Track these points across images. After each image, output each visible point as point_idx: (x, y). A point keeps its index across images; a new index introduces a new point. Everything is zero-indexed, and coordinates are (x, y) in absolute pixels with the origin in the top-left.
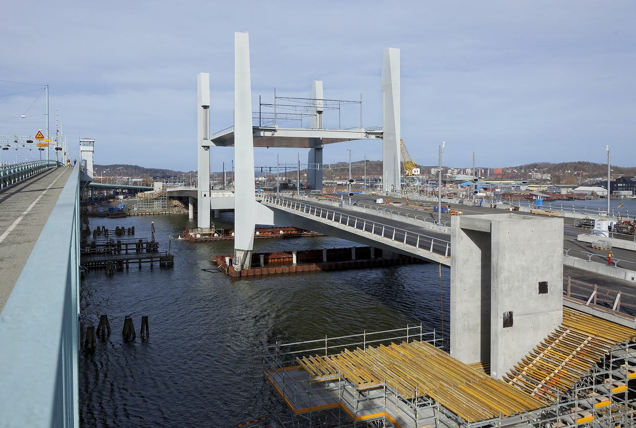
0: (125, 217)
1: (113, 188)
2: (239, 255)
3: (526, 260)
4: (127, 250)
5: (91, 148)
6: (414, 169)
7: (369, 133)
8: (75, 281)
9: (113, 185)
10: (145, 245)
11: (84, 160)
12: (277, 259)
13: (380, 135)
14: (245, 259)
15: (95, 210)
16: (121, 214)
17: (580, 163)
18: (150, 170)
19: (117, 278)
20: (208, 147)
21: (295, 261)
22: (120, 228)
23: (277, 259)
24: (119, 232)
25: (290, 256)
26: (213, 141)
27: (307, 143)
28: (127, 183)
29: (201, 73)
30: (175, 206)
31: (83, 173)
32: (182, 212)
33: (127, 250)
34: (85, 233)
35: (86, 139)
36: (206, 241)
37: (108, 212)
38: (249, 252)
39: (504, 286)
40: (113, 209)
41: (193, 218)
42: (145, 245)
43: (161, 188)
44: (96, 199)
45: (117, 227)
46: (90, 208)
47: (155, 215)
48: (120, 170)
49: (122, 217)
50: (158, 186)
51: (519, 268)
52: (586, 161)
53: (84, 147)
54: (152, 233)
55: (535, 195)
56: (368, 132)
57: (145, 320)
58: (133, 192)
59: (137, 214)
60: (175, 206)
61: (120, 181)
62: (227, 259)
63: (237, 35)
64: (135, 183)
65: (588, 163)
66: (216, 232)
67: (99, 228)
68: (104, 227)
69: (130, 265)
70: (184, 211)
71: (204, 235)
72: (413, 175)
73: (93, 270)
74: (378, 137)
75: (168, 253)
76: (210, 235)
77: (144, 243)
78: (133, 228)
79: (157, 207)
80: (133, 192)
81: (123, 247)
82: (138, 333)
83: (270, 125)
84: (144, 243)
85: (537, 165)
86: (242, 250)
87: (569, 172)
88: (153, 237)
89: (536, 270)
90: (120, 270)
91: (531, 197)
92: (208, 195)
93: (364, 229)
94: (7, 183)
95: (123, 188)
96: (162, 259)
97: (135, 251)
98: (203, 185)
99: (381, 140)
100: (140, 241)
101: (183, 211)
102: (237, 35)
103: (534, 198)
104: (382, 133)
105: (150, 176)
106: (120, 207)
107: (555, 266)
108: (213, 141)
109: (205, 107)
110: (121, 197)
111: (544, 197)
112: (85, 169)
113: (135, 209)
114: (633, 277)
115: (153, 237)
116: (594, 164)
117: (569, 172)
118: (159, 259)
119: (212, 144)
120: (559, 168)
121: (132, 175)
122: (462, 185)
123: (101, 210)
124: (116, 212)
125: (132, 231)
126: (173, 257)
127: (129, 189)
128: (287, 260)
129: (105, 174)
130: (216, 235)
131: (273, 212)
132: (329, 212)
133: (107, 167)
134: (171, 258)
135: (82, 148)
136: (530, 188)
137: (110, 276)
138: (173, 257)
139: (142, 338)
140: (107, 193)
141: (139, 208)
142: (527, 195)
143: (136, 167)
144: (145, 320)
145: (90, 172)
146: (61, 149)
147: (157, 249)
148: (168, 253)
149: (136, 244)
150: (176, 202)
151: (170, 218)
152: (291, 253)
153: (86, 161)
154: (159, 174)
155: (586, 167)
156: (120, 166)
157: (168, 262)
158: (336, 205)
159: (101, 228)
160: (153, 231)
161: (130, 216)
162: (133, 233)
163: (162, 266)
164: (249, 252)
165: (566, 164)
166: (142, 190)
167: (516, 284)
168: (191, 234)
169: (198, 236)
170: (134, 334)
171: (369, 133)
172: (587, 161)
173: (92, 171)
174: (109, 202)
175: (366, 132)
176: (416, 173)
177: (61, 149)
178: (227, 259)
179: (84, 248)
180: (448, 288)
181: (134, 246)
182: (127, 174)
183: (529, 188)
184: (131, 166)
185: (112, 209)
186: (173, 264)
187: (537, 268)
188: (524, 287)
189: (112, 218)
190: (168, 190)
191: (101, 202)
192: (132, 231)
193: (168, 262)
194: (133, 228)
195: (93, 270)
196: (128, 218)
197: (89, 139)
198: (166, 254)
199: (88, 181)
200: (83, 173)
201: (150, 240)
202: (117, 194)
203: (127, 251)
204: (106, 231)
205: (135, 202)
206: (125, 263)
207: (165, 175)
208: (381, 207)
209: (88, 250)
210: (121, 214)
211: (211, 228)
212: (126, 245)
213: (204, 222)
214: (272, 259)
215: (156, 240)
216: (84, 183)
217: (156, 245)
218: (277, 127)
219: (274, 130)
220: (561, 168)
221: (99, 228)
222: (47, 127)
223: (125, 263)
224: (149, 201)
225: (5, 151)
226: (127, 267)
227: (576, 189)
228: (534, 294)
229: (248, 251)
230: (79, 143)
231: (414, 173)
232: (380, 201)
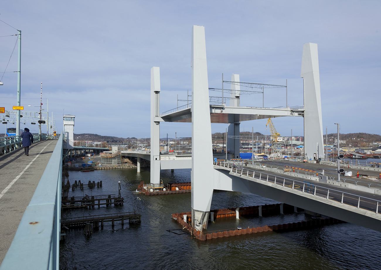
0: (93, 171)
1: (84, 149)
2: (198, 216)
4: (99, 205)
5: (72, 123)
6: (278, 138)
7: (294, 111)
8: (59, 202)
9: (84, 147)
10: (113, 201)
11: (66, 132)
12: (223, 214)
13: (302, 113)
14: (203, 219)
15: (73, 166)
16: (90, 169)
17: (360, 134)
19: (95, 238)
20: (159, 122)
21: (238, 217)
22: (92, 182)
23: (223, 214)
24: (91, 186)
25: (233, 212)
26: (163, 118)
27: (227, 118)
29: (154, 67)
30: (126, 163)
31: (65, 143)
32: (131, 167)
33: (99, 205)
34: (65, 188)
35: (69, 115)
36: (158, 195)
37: (82, 167)
38: (207, 214)
40: (85, 165)
41: (140, 172)
43: (117, 151)
44: (73, 156)
45: (90, 182)
46: (69, 164)
47: (114, 170)
49: (91, 171)
50: (115, 149)
52: (364, 132)
53: (67, 122)
54: (119, 190)
55: (354, 155)
56: (293, 110)
58: (97, 152)
59: (101, 168)
60: (126, 163)
61: (88, 143)
62: (185, 217)
63: (196, 27)
64: (97, 145)
65: (365, 134)
66: (164, 187)
67: (76, 182)
68: (80, 181)
70: (133, 166)
71: (156, 189)
72: (278, 141)
73: (73, 230)
74: (300, 114)
76: (160, 189)
78: (101, 182)
79: (114, 164)
80: (97, 152)
81: (96, 202)
83: (220, 105)
85: (333, 135)
86: (201, 211)
87: (354, 139)
88: (120, 193)
90: (96, 229)
92: (158, 159)
94: (10, 150)
95: (90, 149)
97: (105, 206)
98: (154, 151)
101: (133, 166)
102: (196, 27)
103: (354, 157)
104: (303, 112)
105: (105, 140)
106: (89, 163)
108: (163, 118)
109: (157, 92)
110: (89, 155)
111: (360, 156)
112: (68, 140)
113: (100, 165)
115: (120, 193)
116: (369, 134)
117: (354, 139)
119: (161, 120)
120: (348, 137)
121: (94, 140)
122: (297, 147)
123: (77, 165)
124: (87, 167)
125: (100, 185)
127: (94, 150)
128: (231, 215)
129: (78, 139)
130: (164, 189)
131: (232, 179)
132: (277, 177)
133: (79, 135)
134: (138, 217)
135: (65, 122)
136: (344, 150)
137: (88, 237)
140: (80, 152)
141: (102, 164)
142: (349, 155)
143: (96, 135)
145: (71, 142)
146: (44, 122)
147: (123, 203)
150: (126, 160)
151: (123, 172)
152: (234, 210)
153: (68, 133)
154: (109, 140)
155: (365, 136)
156: (87, 134)
158: (315, 179)
159: (78, 182)
160: (120, 189)
161: (96, 169)
162: (101, 186)
163: (131, 224)
164: (207, 214)
165: (352, 134)
168: (145, 188)
169: (152, 190)
171: (294, 111)
172: (365, 133)
173: (73, 141)
174: (82, 159)
175: (292, 111)
176: (279, 141)
177: (44, 122)
178: (185, 217)
179: (65, 204)
180: (190, 175)
181: (105, 202)
182: (90, 140)
183: (342, 150)
184: (93, 135)
185: (84, 165)
186: (140, 222)
189: (84, 172)
190: (122, 152)
191: (76, 159)
192: (100, 185)
194: (101, 182)
195: (73, 230)
196: (95, 171)
197: (70, 115)
199: (69, 149)
200: (65, 143)
201: (117, 196)
202: (87, 153)
203: (99, 206)
204: (82, 185)
205: (99, 159)
206: (100, 222)
207: (114, 141)
208: (350, 180)
209: (68, 205)
210: (90, 169)
211: (160, 184)
212: (99, 200)
213: (155, 178)
214: (219, 215)
215: (122, 196)
216: (65, 150)
217: (122, 200)
218: (225, 105)
219: (222, 108)
220: (349, 137)
221: (76, 182)
222: (18, 90)
224: (109, 159)
225: (33, 125)
226: (102, 226)
227: (376, 151)
229: (206, 212)
230: (63, 118)
231: (278, 141)
232: (349, 174)
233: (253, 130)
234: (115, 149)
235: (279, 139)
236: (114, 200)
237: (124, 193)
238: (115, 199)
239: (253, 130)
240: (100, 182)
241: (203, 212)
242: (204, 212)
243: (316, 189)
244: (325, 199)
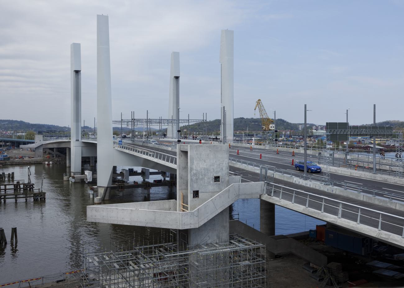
3: (206, 165)
4: (5, 190)
10: (22, 186)
18: (35, 125)
28: (11, 137)
33: (5, 190)
39: (193, 178)
42: (22, 186)
48: (4, 125)
51: (202, 169)
54: (29, 175)
57: (14, 230)
64: (20, 137)
69: (8, 201)
72: (270, 130)
75: (40, 190)
77: (21, 184)
82: (8, 239)
84: (21, 184)
86: (103, 187)
88: (29, 179)
89: (212, 170)
91: (369, 149)
93: (170, 162)
96: (35, 195)
99: (263, 102)
100: (18, 182)
107: (224, 168)
114: (398, 205)
115: (29, 179)
118: (33, 195)
126: (45, 193)
138: (45, 193)
139: (12, 245)
143: (21, 123)
144: (14, 230)
147: (33, 189)
148: (40, 190)
149: (14, 185)
157: (41, 197)
160: (29, 174)
163: (36, 201)
164: (109, 188)
166: (25, 143)
167: (201, 177)
170: (5, 240)
176: (272, 128)
187: (213, 169)
188: (206, 178)
193: (41, 197)
198: (39, 191)
206: (2, 198)
217: (32, 186)
223: (2, 198)
226: (5, 201)
228: (212, 182)
231: (271, 129)
233: (275, 118)
234: (39, 140)
235: (271, 127)
236: (23, 185)
237: (88, 278)
238: (24, 184)
239: (275, 118)
240: (11, 173)
241: (105, 187)
242: (105, 187)
243: (359, 214)
244: (320, 212)
